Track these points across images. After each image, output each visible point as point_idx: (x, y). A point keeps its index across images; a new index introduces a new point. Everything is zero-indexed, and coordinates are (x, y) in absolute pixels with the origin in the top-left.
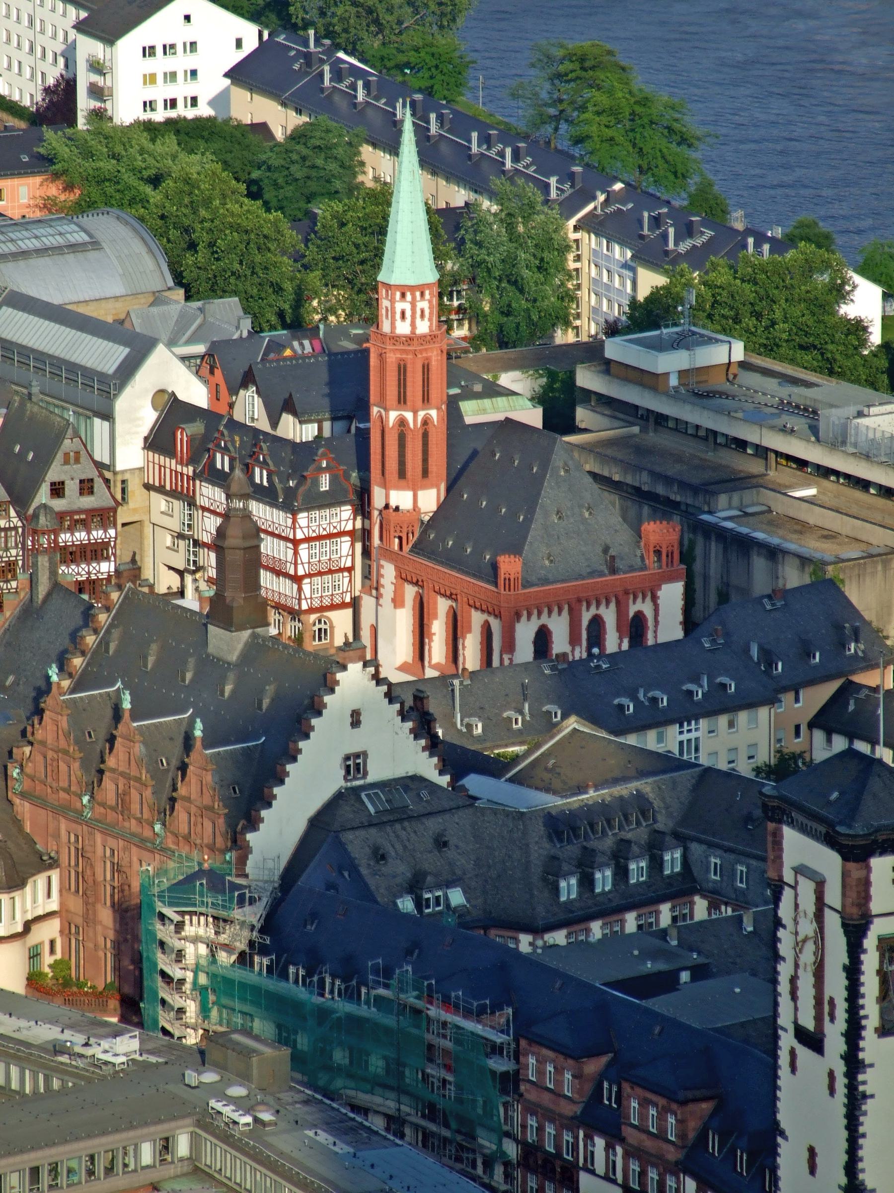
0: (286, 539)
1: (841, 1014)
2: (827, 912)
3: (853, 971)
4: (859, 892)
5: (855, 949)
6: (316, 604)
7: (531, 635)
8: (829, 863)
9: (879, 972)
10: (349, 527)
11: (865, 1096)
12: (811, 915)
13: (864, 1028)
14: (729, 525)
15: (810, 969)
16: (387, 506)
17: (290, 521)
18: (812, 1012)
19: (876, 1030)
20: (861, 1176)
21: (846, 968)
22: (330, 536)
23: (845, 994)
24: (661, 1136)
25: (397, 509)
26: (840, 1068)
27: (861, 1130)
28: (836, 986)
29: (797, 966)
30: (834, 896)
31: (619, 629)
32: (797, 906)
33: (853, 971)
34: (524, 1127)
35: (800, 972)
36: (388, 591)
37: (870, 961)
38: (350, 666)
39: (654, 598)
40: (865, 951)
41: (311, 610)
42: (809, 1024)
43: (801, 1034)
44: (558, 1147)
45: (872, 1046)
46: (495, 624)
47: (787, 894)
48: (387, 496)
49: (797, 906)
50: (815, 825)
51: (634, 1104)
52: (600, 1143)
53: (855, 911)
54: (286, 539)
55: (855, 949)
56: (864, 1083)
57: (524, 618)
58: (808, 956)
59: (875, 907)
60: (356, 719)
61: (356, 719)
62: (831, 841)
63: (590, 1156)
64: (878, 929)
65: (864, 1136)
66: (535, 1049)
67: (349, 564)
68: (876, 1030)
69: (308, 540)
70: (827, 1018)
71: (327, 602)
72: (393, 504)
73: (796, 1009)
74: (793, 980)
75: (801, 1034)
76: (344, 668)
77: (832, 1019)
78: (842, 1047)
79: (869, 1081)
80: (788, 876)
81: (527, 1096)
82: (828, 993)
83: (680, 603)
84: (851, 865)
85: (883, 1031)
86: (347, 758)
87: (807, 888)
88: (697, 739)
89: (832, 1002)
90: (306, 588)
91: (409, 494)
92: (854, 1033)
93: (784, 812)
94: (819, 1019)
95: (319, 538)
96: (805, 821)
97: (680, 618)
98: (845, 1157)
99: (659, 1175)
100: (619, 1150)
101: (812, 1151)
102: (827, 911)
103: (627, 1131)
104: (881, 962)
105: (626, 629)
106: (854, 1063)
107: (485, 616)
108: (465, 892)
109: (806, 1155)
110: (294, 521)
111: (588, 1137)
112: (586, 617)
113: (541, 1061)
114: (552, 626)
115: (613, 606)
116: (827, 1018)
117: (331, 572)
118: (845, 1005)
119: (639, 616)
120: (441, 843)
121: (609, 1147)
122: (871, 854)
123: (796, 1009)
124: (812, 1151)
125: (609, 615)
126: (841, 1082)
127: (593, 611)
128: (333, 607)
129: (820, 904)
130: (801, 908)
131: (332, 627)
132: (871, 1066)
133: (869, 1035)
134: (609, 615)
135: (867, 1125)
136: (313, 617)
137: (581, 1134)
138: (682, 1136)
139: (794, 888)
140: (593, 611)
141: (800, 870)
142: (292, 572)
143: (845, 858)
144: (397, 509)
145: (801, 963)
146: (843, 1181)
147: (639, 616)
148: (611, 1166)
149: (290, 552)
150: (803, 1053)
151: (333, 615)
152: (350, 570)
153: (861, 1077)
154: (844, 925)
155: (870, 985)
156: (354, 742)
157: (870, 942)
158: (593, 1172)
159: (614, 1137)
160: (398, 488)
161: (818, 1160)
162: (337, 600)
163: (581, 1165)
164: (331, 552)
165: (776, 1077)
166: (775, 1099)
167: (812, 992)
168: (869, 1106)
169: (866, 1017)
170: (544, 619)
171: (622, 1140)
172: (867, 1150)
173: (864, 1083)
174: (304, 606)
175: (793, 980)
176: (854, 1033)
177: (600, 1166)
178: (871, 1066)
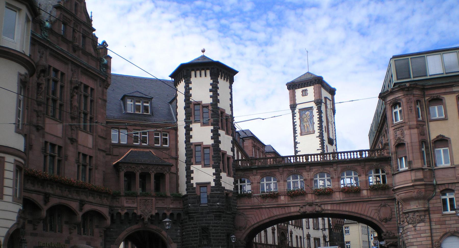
45: (299, 138)
59: (297, 102)
64: (299, 107)
85: (301, 134)
157: (297, 111)
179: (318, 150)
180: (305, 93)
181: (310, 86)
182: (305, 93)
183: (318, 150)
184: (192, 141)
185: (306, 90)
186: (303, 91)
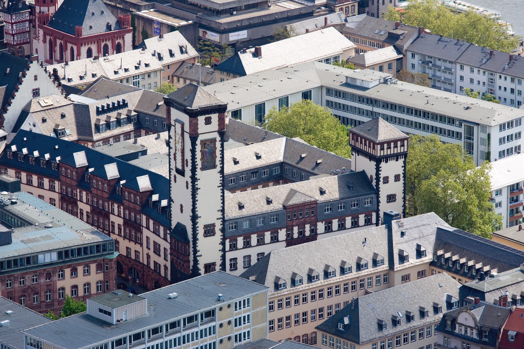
0: (9, 23)
1: (190, 164)
2: (185, 133)
3: (193, 151)
4: (194, 127)
5: (194, 144)
6: (19, 42)
7: (86, 51)
8: (185, 118)
9: (201, 151)
10: (28, 18)
11: (197, 189)
12: (180, 134)
13: (197, 168)
14: (145, 15)
15: (180, 151)
16: (40, 12)
17: (10, 17)
18: (181, 164)
19: (200, 169)
20: (197, 213)
21: (191, 150)
22: (22, 21)
23: (191, 158)
24: (135, 203)
25: (43, 13)
26: (190, 181)
27: (196, 199)
28: (188, 155)
29: (176, 150)
30: (187, 128)
31: (113, 48)
32: (175, 132)
33: (193, 151)
34: (92, 201)
35: (177, 152)
36: (41, 38)
37: (198, 148)
38: (34, 62)
39: (123, 38)
40: (197, 145)
41: (17, 45)
42: (180, 167)
43: (177, 171)
44: (67, 193)
45: (199, 174)
46: (75, 48)
47: (173, 128)
48: (40, 9)
49: (175, 132)
50: (180, 107)
51: (127, 193)
52: (116, 206)
53: (193, 133)
54: (9, 23)
55: (194, 144)
56: (197, 185)
57: (83, 45)
58: (179, 147)
59: (199, 131)
60: (36, 78)
61: (36, 78)
62: (186, 111)
63: (113, 210)
64: (201, 138)
65: (197, 201)
66: (95, 178)
67: (28, 30)
68: (200, 169)
69: (15, 23)
70: (185, 166)
71: (22, 42)
72: (42, 11)
73: (176, 163)
74: (175, 154)
75: (177, 171)
76: (32, 62)
77: (187, 166)
78: (190, 174)
79: (199, 184)
80: (173, 123)
81: (93, 192)
82: (186, 158)
83: (131, 39)
84: (192, 119)
85: (202, 169)
86: (34, 90)
87: (178, 126)
88: (139, 81)
89: (187, 160)
90: (16, 38)
91: (47, 8)
92: (194, 170)
93: (171, 103)
94: (183, 166)
95: (19, 22)
96: (178, 106)
97: (132, 44)
98: (192, 207)
99: (135, 214)
100: (122, 207)
101: (181, 206)
102: (185, 133)
103: (124, 201)
104: (202, 148)
105: (114, 48)
106: (194, 179)
107: (72, 45)
108: (334, 219)
109: (180, 207)
110: (11, 17)
111: (112, 204)
112: (103, 45)
113: (97, 181)
114: (92, 48)
115: (110, 41)
116: (185, 166)
117: (23, 33)
118: (191, 161)
119: (119, 43)
120: (63, 116)
121: (87, 194)
122: (198, 116)
123: (176, 163)
124: (181, 206)
125: (109, 44)
126: (190, 185)
127: (104, 42)
128: (24, 43)
129: (183, 131)
130: (177, 132)
131: (24, 50)
132: (199, 179)
133: (198, 170)
134: (109, 44)
135: (198, 197)
136: (18, 47)
137: (78, 190)
138: (141, 202)
139: (175, 126)
140: (104, 42)
141: (177, 121)
142: (11, 33)
143: (190, 117)
144: (43, 13)
145: (177, 149)
146: (191, 214)
147: (119, 43)
148: (119, 212)
149: (10, 27)
150: (178, 176)
151: (24, 46)
152: (29, 32)
153: (196, 183)
154: (190, 137)
155: (198, 155)
156: (36, 85)
157: (198, 142)
158: (114, 214)
159: (120, 203)
160: (43, 6)
161: (183, 208)
162: (25, 41)
163: (79, 199)
164: (23, 26)
165: (170, 184)
166: (170, 190)
167: (181, 158)
168: (199, 192)
169: (197, 165)
170: (90, 45)
171: (123, 204)
172: (198, 205)
173: (197, 185)
174: (15, 43)
175: (175, 154)
176: (194, 170)
177: (116, 212)
178: (199, 179)
179: (218, 187)
180: (208, 121)
181: (215, 113)
182: (208, 121)
183: (218, 187)
184: (403, 160)
185: (210, 118)
186: (206, 119)
